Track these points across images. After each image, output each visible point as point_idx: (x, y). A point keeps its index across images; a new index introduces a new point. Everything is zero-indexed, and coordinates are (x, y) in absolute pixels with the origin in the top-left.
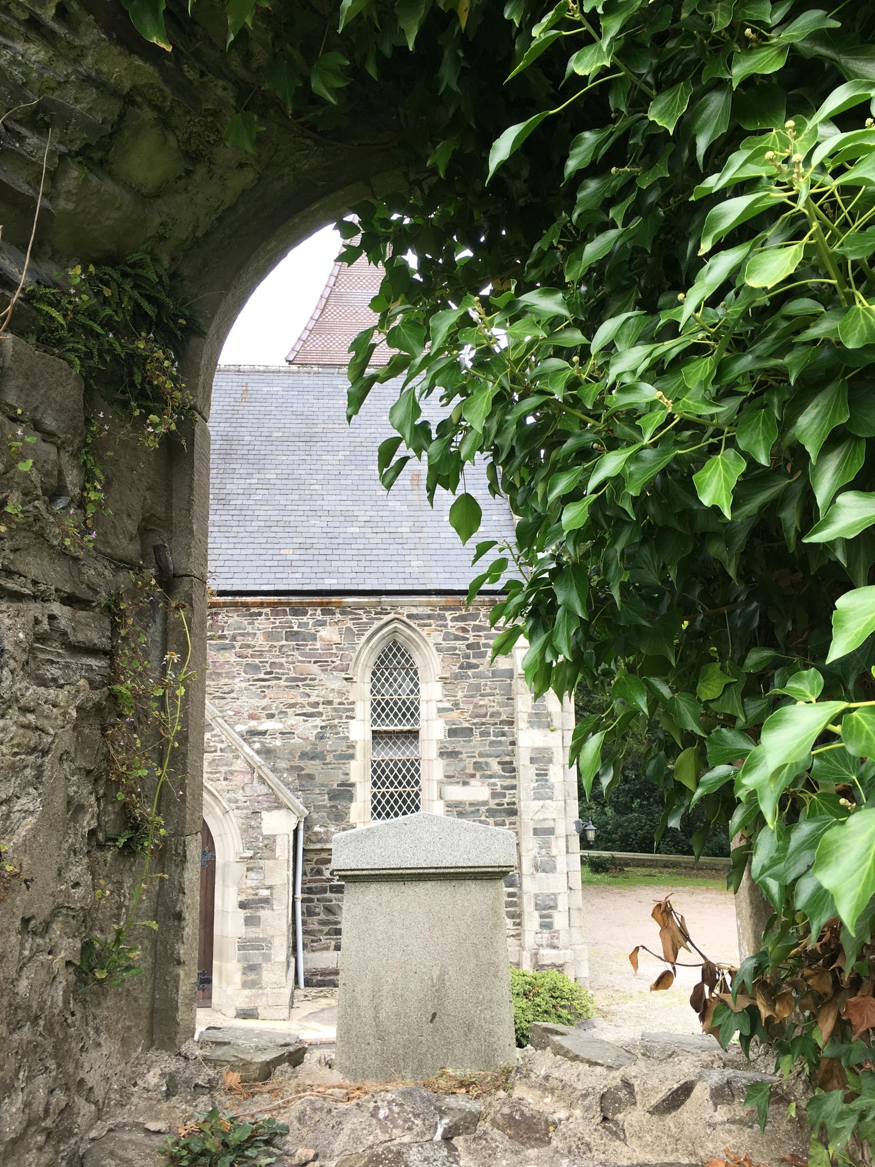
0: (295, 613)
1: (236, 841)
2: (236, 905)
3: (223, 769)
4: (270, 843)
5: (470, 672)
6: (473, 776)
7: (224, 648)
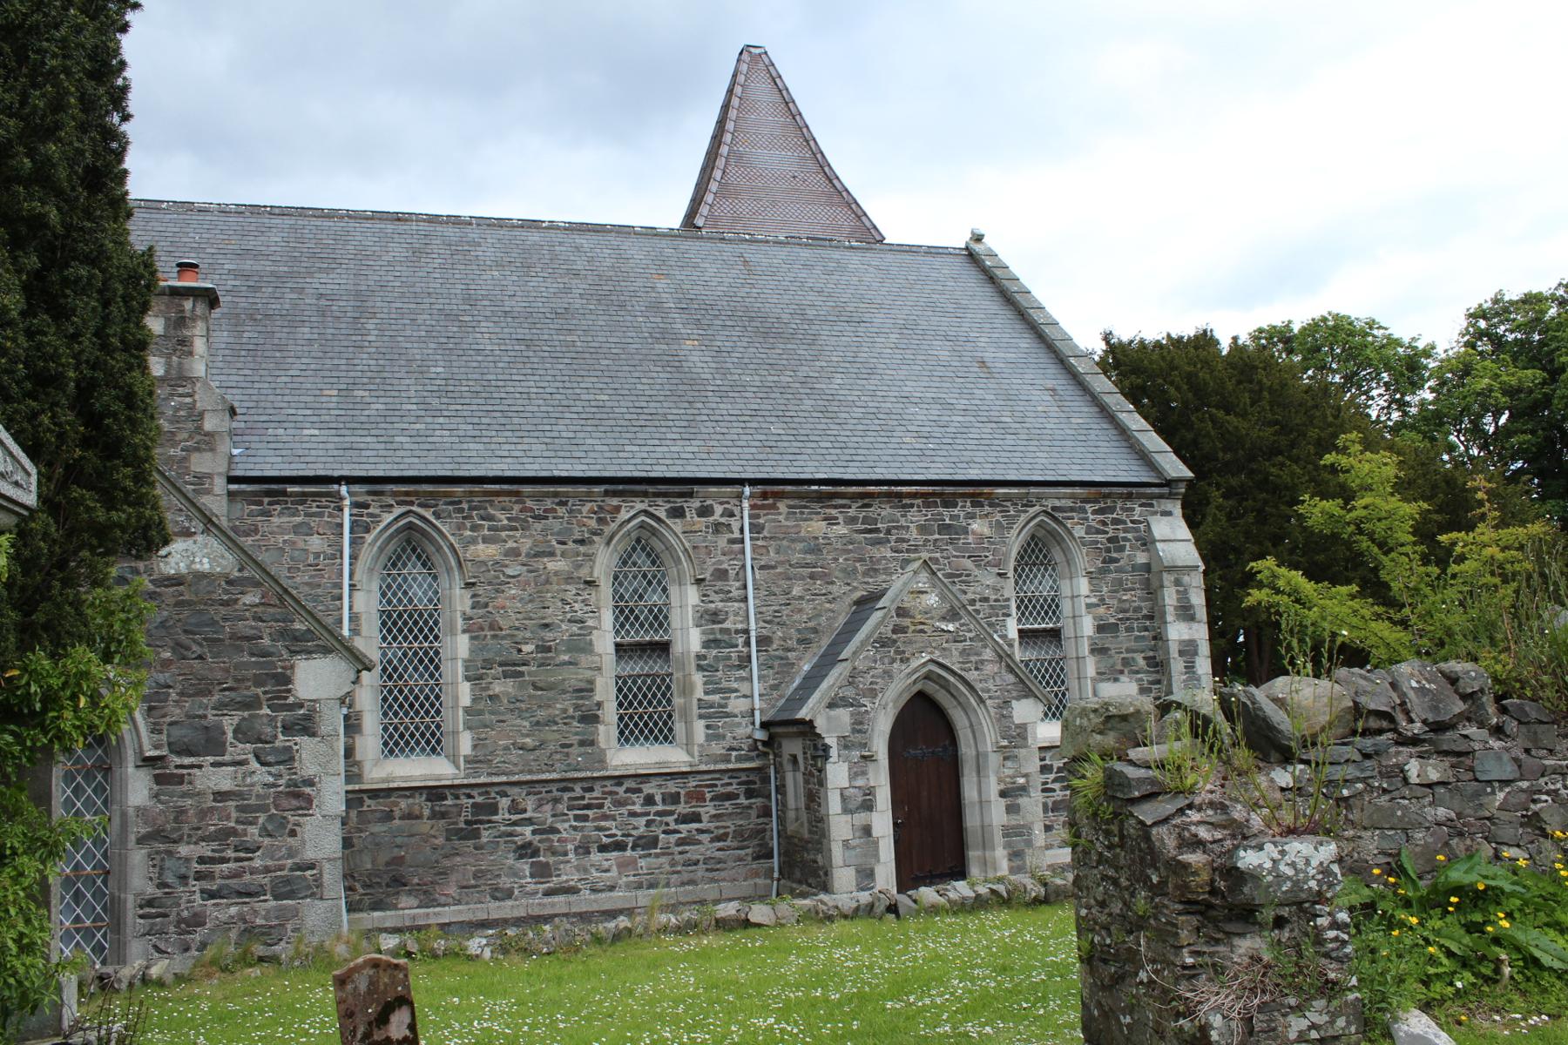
0: (946, 505)
3: (973, 659)
5: (1112, 567)
6: (1122, 672)
7: (879, 542)
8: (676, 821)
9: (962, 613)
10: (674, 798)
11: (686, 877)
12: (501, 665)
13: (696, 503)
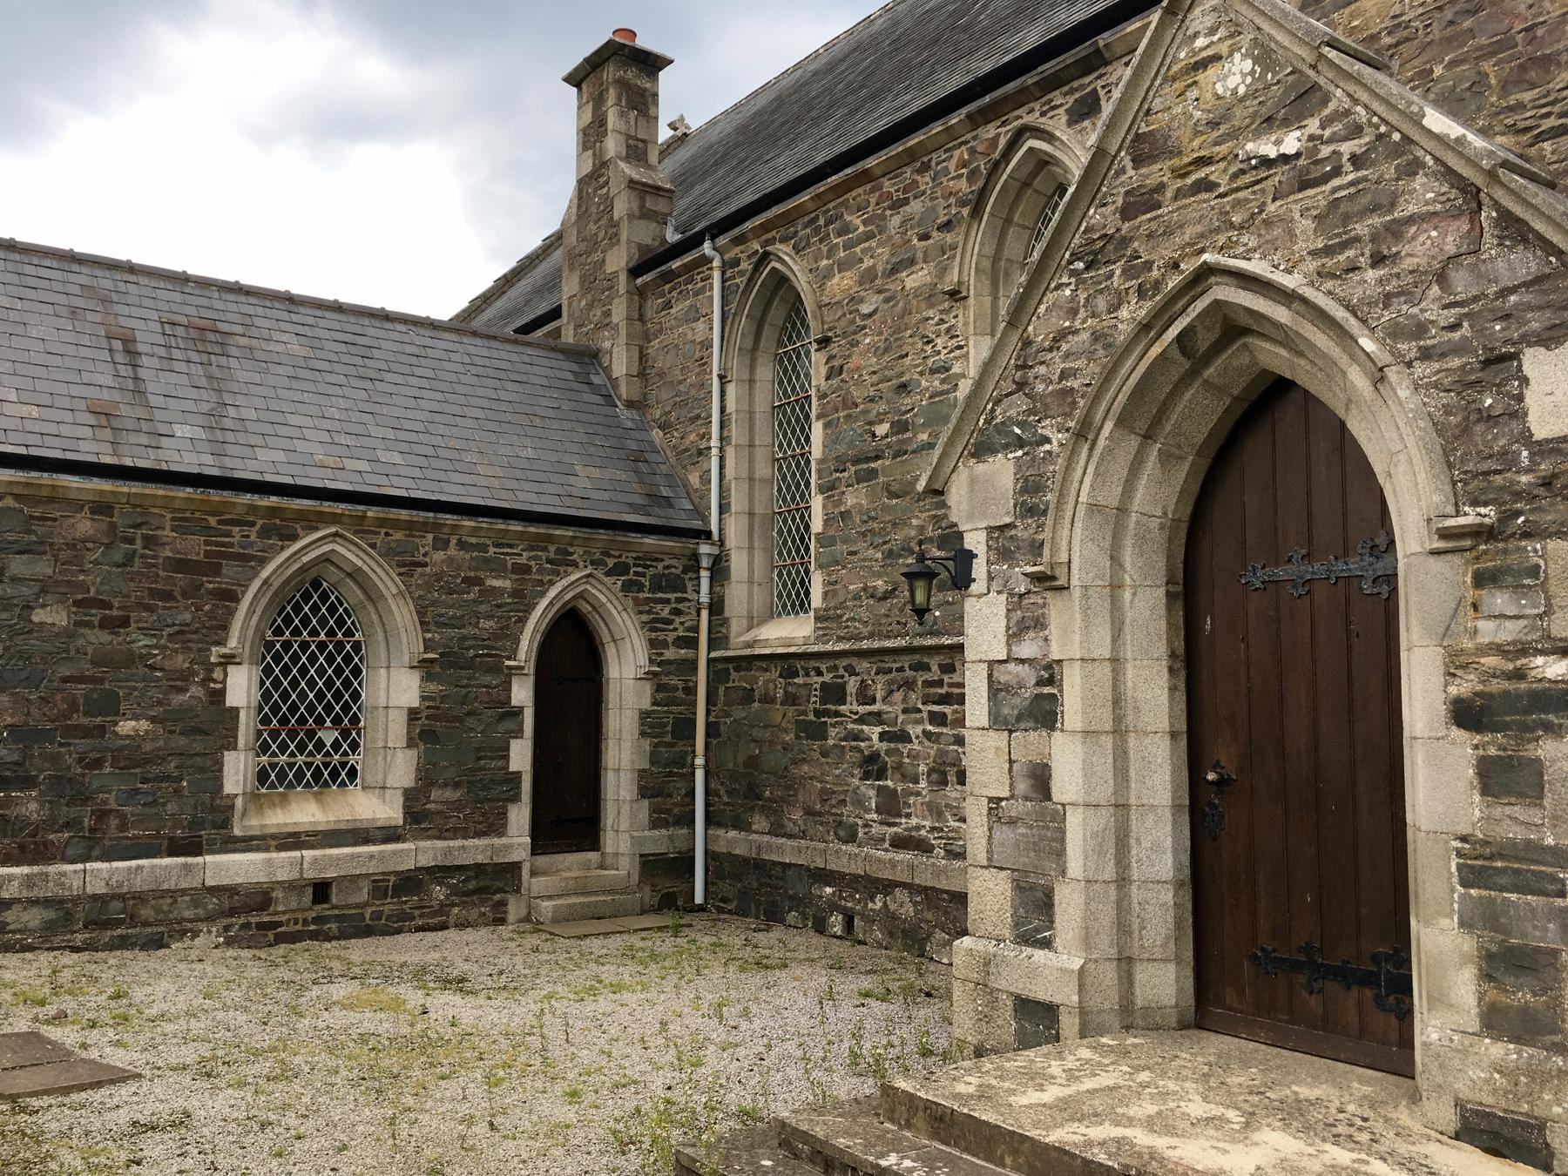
12: (856, 462)
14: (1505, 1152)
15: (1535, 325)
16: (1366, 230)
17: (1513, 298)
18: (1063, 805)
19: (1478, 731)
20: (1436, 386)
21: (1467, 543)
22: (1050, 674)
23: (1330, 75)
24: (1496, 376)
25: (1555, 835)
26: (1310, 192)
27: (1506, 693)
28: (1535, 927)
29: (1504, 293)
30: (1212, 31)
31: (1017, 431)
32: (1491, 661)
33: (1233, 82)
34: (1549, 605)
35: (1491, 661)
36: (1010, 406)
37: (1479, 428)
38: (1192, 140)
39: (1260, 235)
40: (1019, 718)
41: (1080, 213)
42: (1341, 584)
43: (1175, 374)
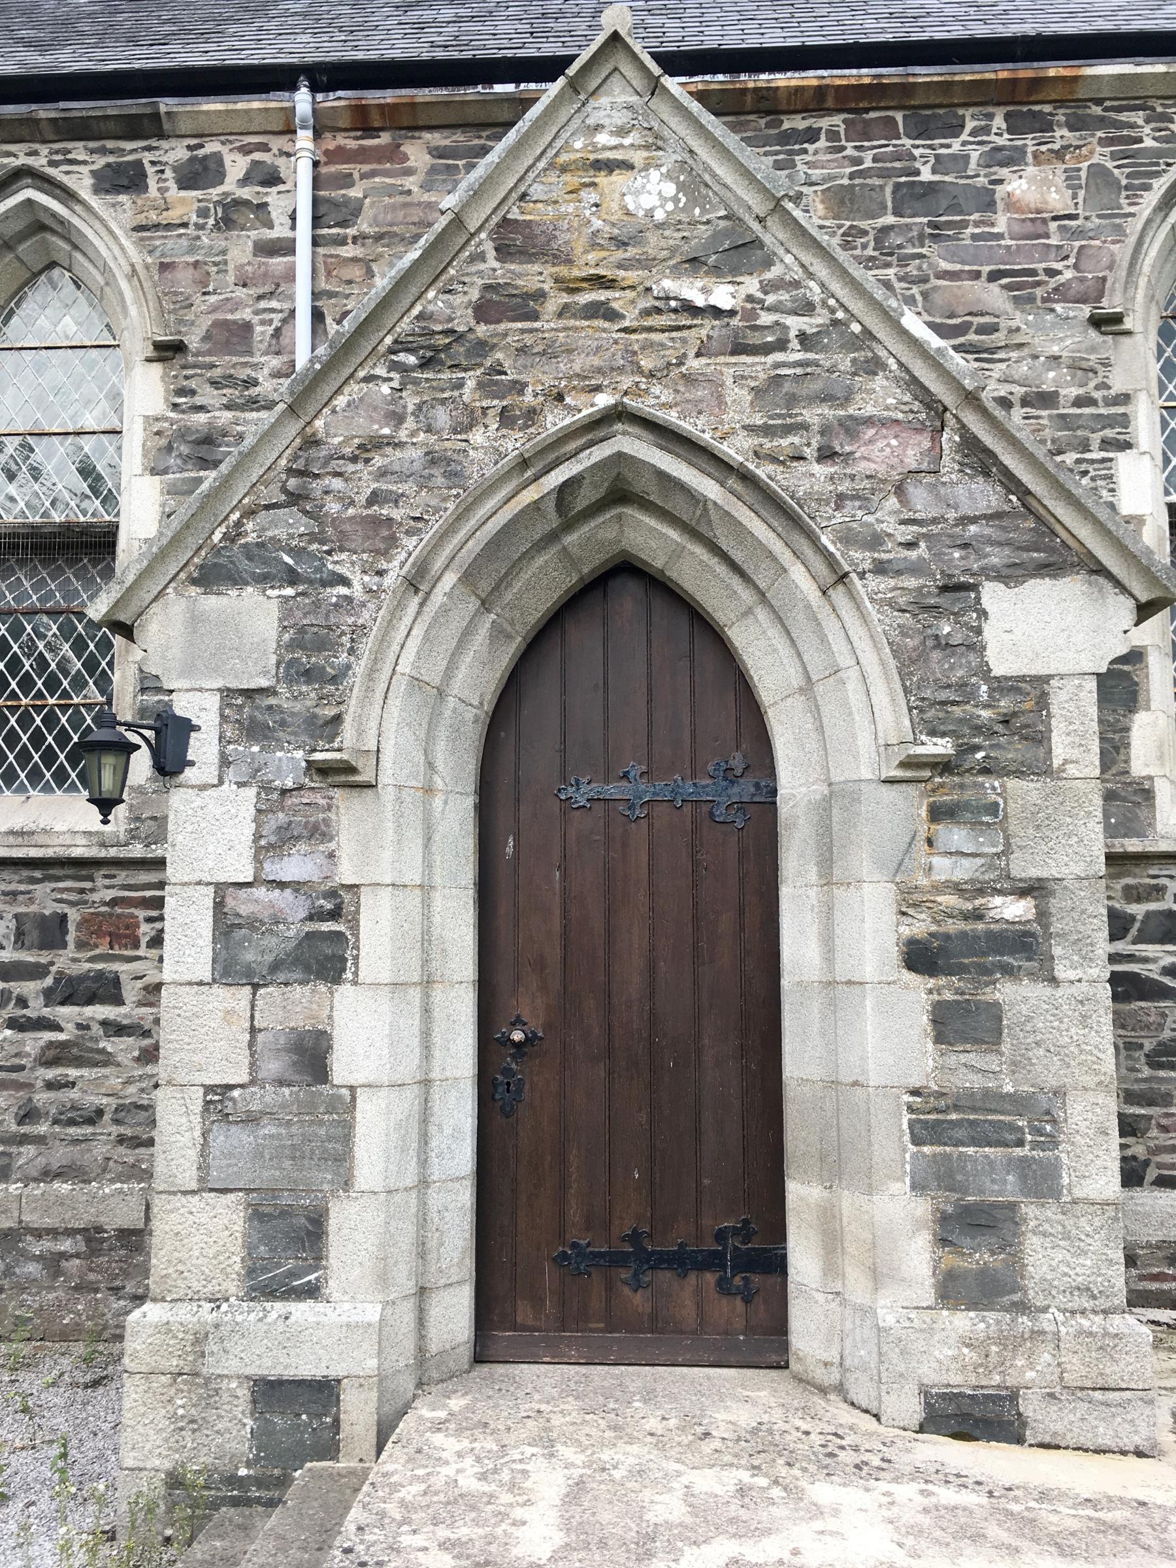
0: (922, 131)
1: (881, 697)
2: (894, 954)
3: (812, 415)
4: (1024, 708)
8: (49, 996)
9: (773, 236)
10: (51, 932)
11: (60, 1155)
13: (176, 152)
14: (977, 1433)
15: (995, 560)
16: (816, 420)
17: (973, 528)
18: (352, 1089)
19: (931, 976)
20: (891, 603)
21: (927, 773)
22: (336, 905)
23: (780, 236)
24: (953, 604)
25: (1015, 1083)
26: (744, 359)
27: (963, 934)
28: (993, 1181)
29: (965, 521)
30: (622, 132)
31: (288, 559)
32: (949, 900)
33: (649, 201)
34: (1007, 844)
35: (949, 900)
36: (274, 523)
37: (936, 655)
38: (586, 252)
39: (677, 391)
40: (275, 967)
41: (414, 291)
42: (687, 809)
43: (539, 530)
